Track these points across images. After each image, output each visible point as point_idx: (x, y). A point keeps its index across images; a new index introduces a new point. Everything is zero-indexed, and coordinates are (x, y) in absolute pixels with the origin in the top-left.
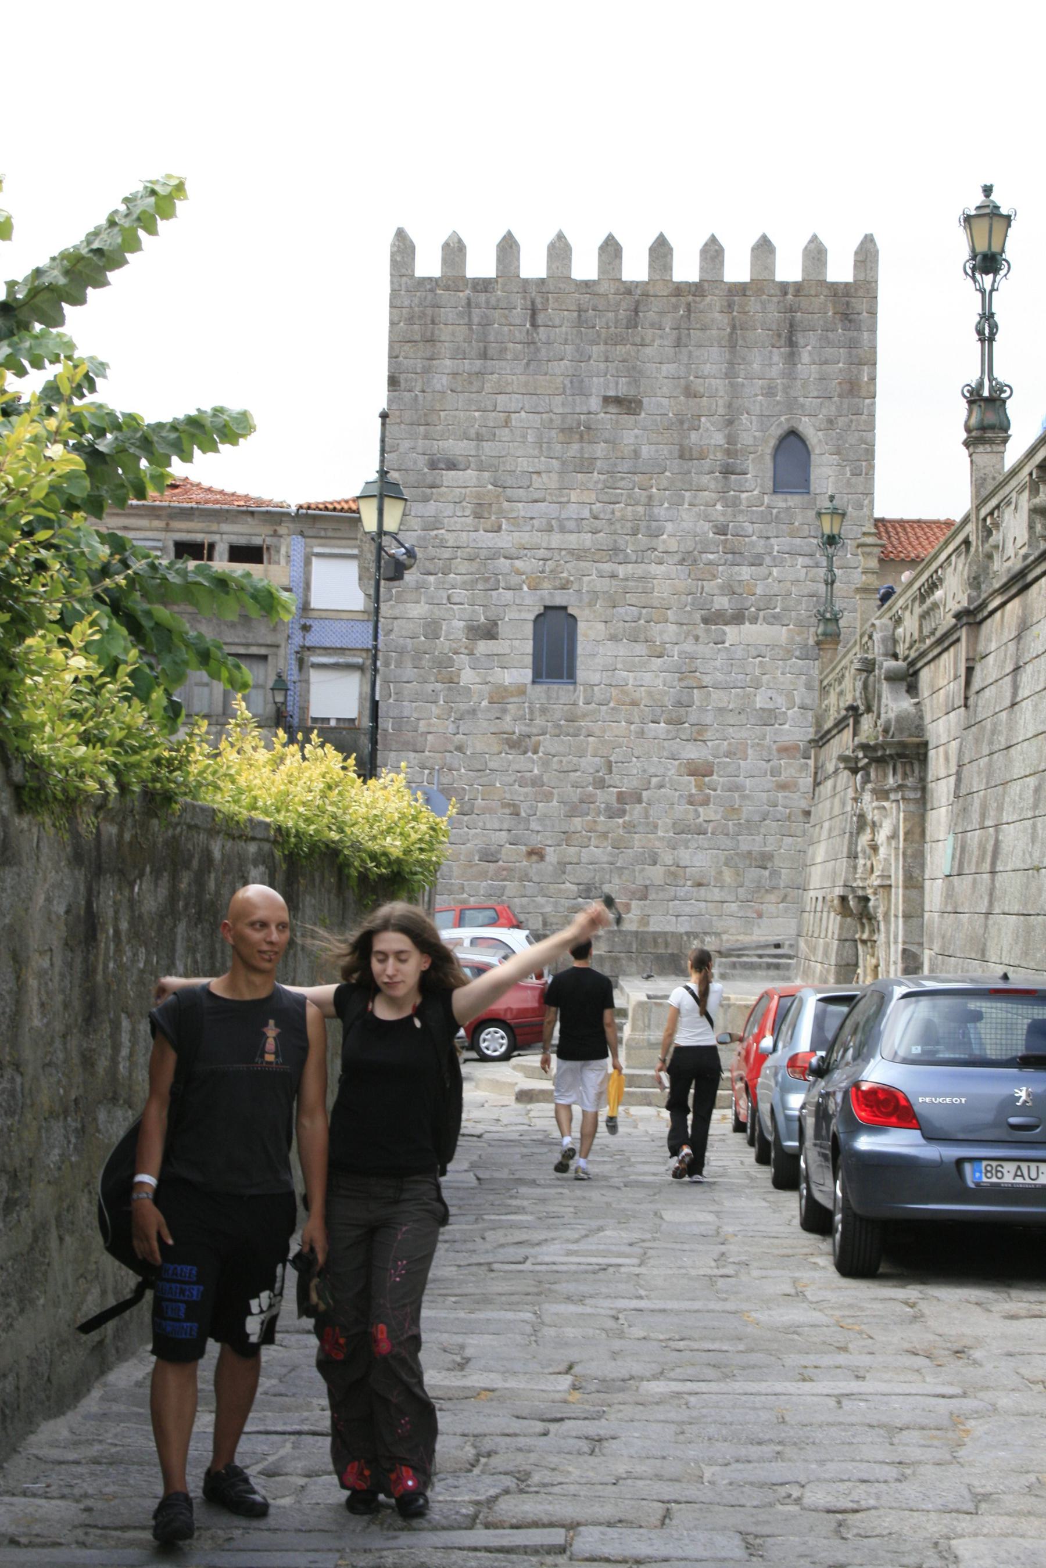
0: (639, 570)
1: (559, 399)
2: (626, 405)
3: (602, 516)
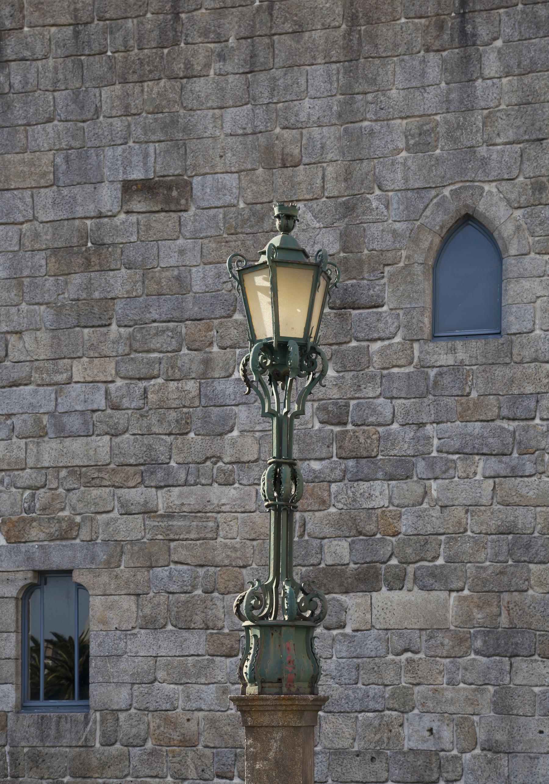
0: (191, 497)
1: (46, 195)
2: (163, 193)
3: (126, 403)
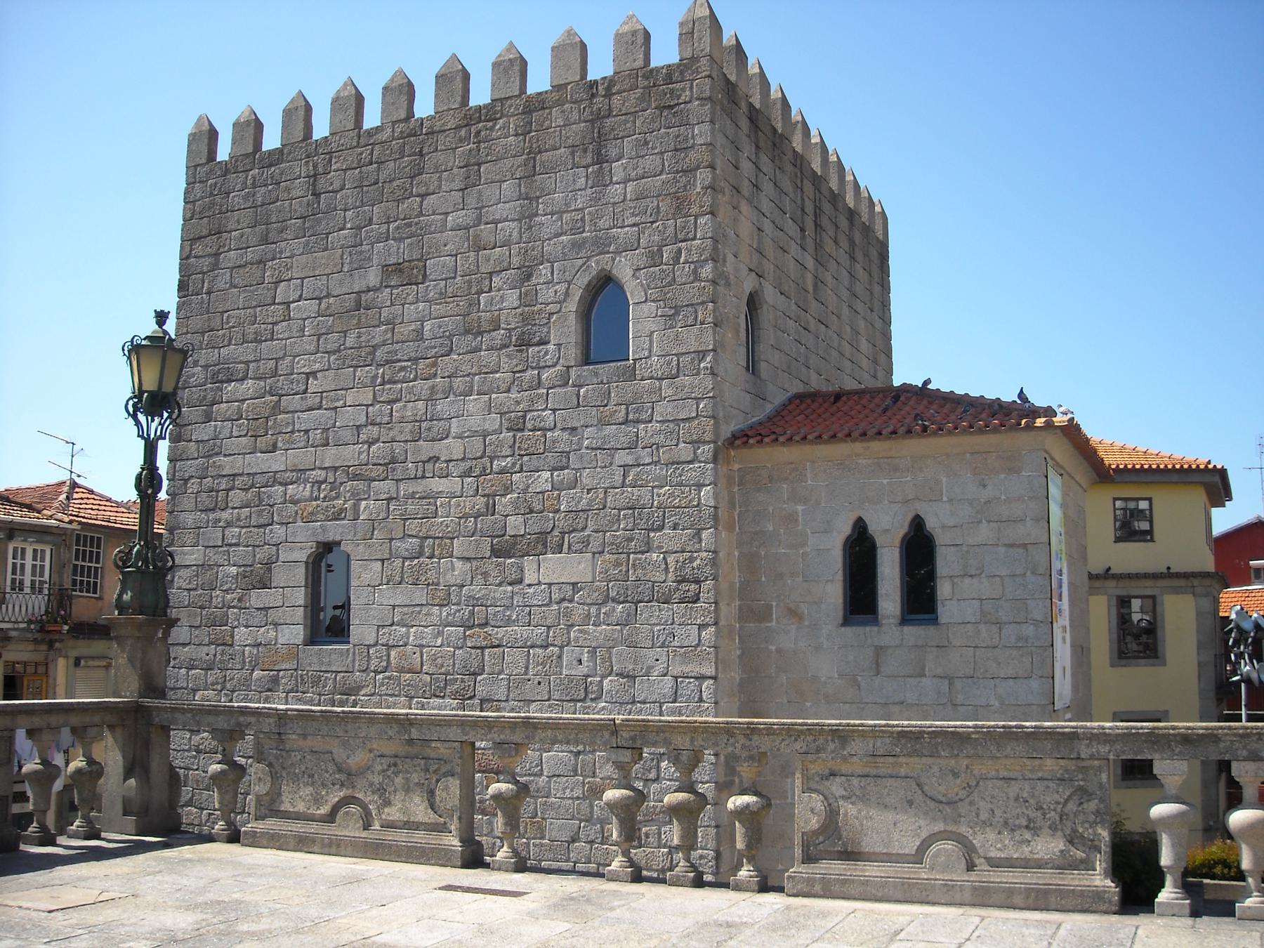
2: (406, 273)
